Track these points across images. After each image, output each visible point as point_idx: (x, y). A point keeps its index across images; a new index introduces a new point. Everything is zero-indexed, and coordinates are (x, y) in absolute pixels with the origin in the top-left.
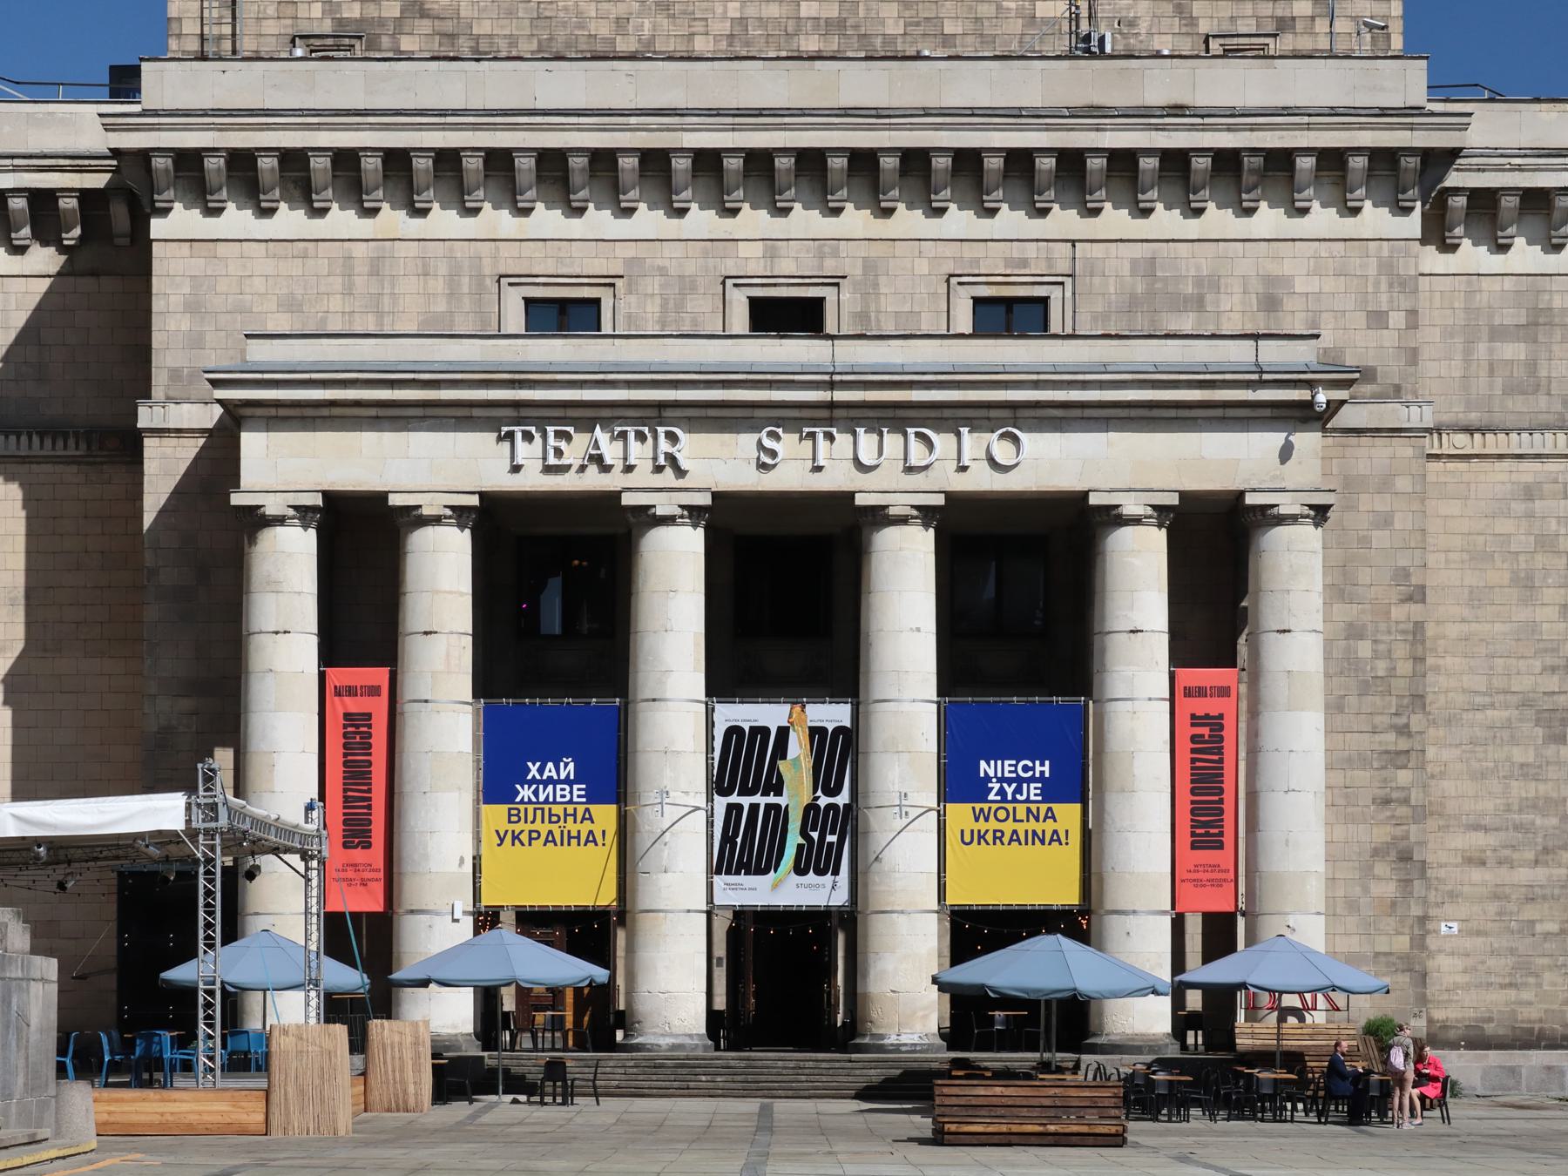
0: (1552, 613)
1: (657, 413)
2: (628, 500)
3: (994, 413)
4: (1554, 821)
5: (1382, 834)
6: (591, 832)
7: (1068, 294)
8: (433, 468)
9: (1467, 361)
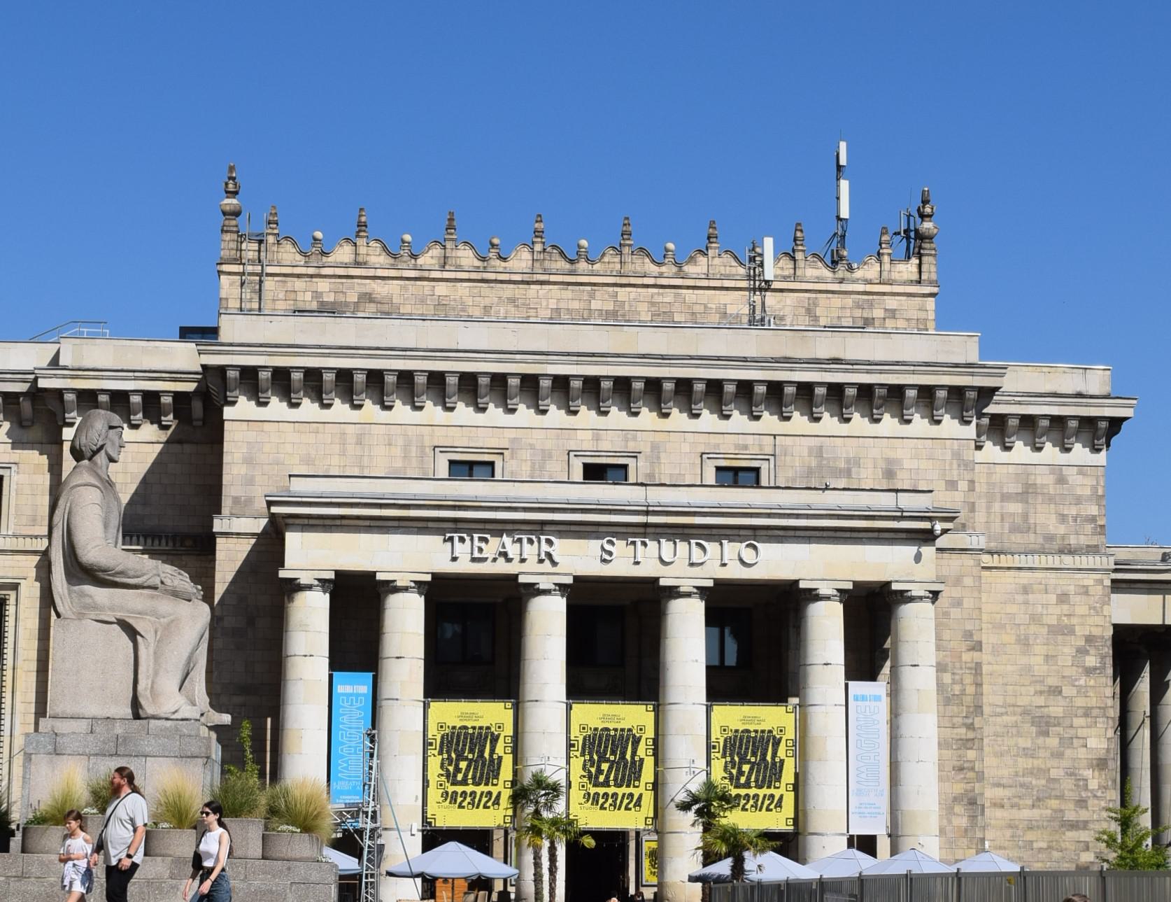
0: (1040, 660)
1: (540, 527)
2: (522, 579)
3: (742, 532)
4: (1043, 782)
5: (959, 788)
7: (772, 466)
8: (405, 559)
9: (989, 513)
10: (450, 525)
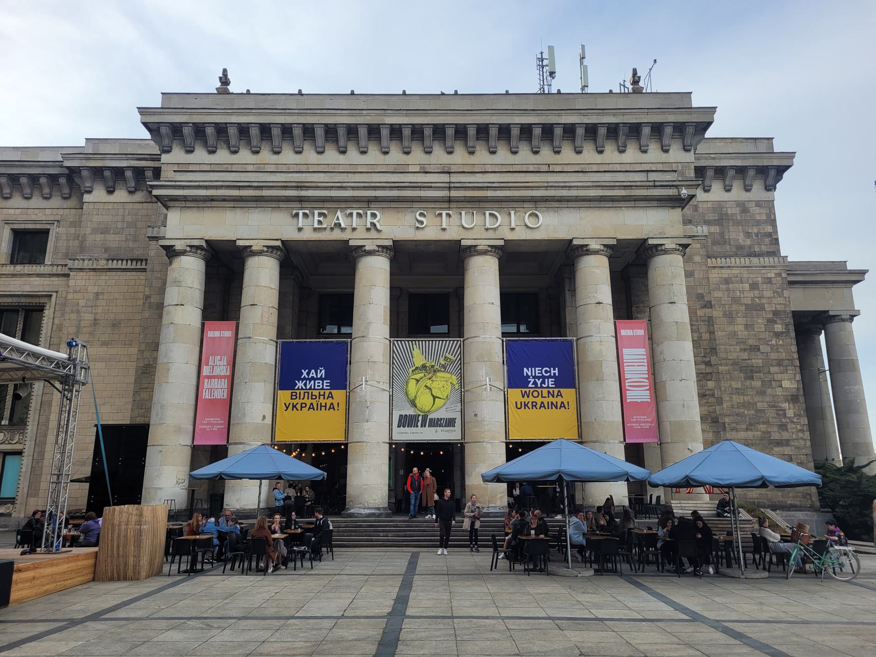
0: (741, 327)
4: (753, 412)
6: (332, 404)
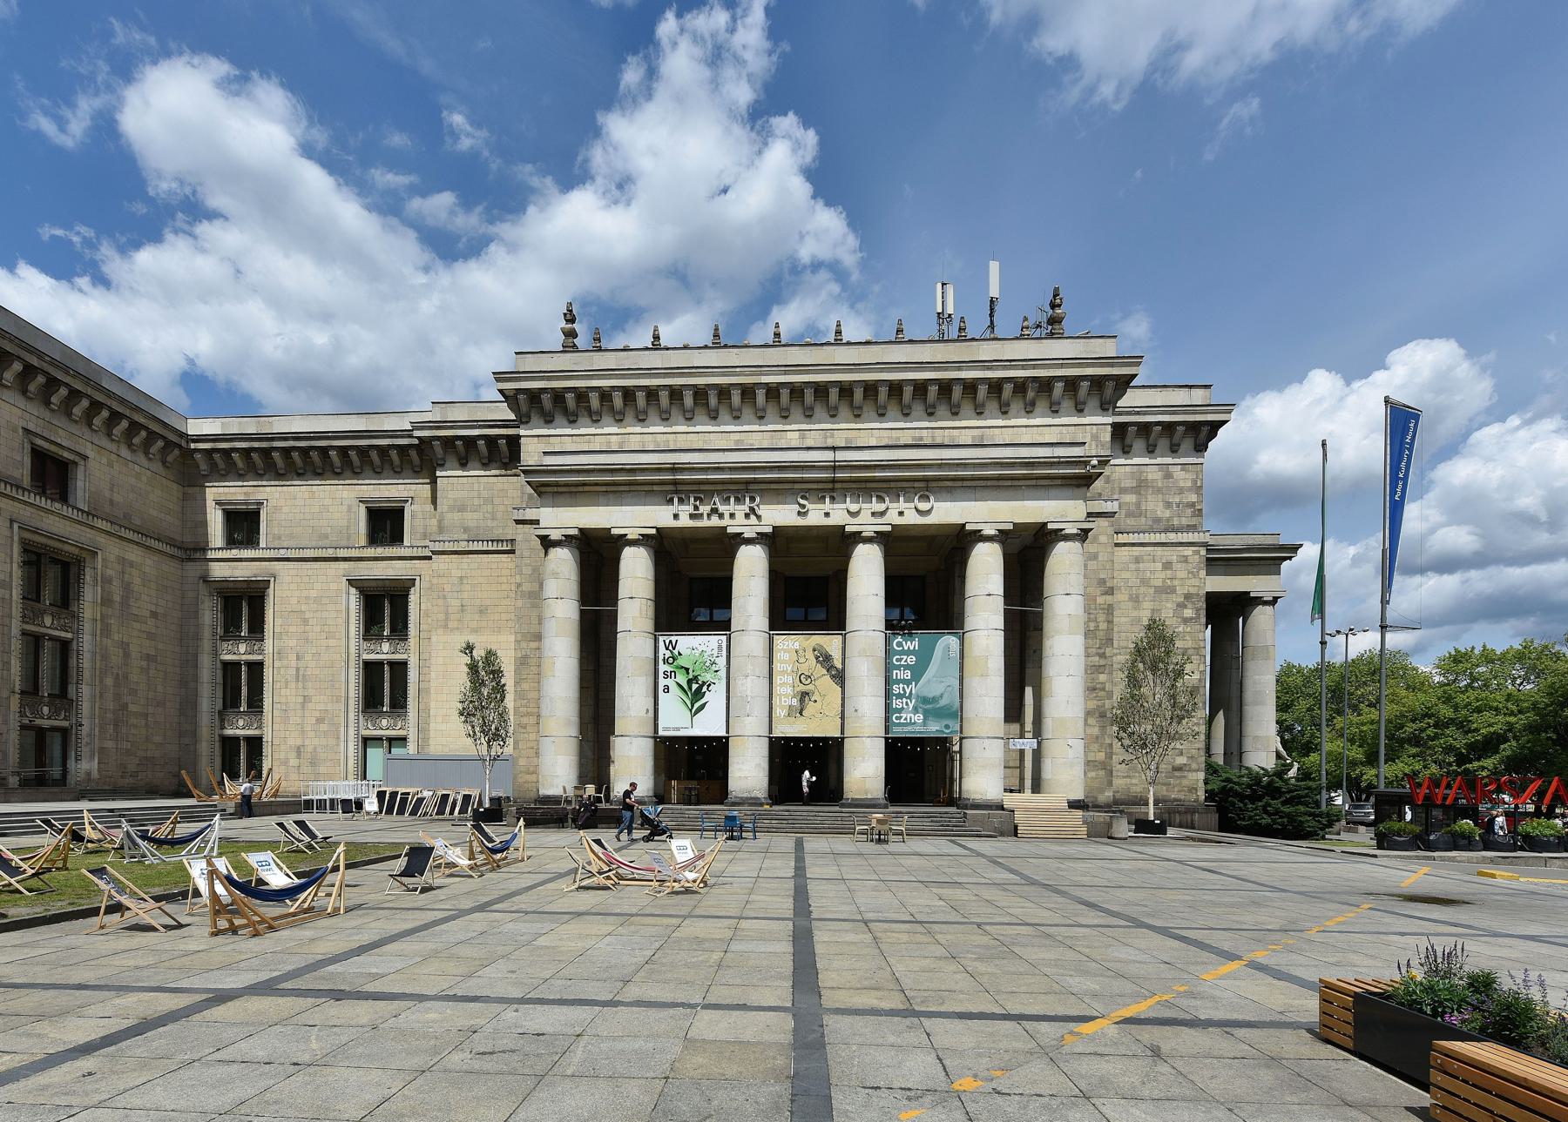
5: (1092, 704)
10: (671, 488)
